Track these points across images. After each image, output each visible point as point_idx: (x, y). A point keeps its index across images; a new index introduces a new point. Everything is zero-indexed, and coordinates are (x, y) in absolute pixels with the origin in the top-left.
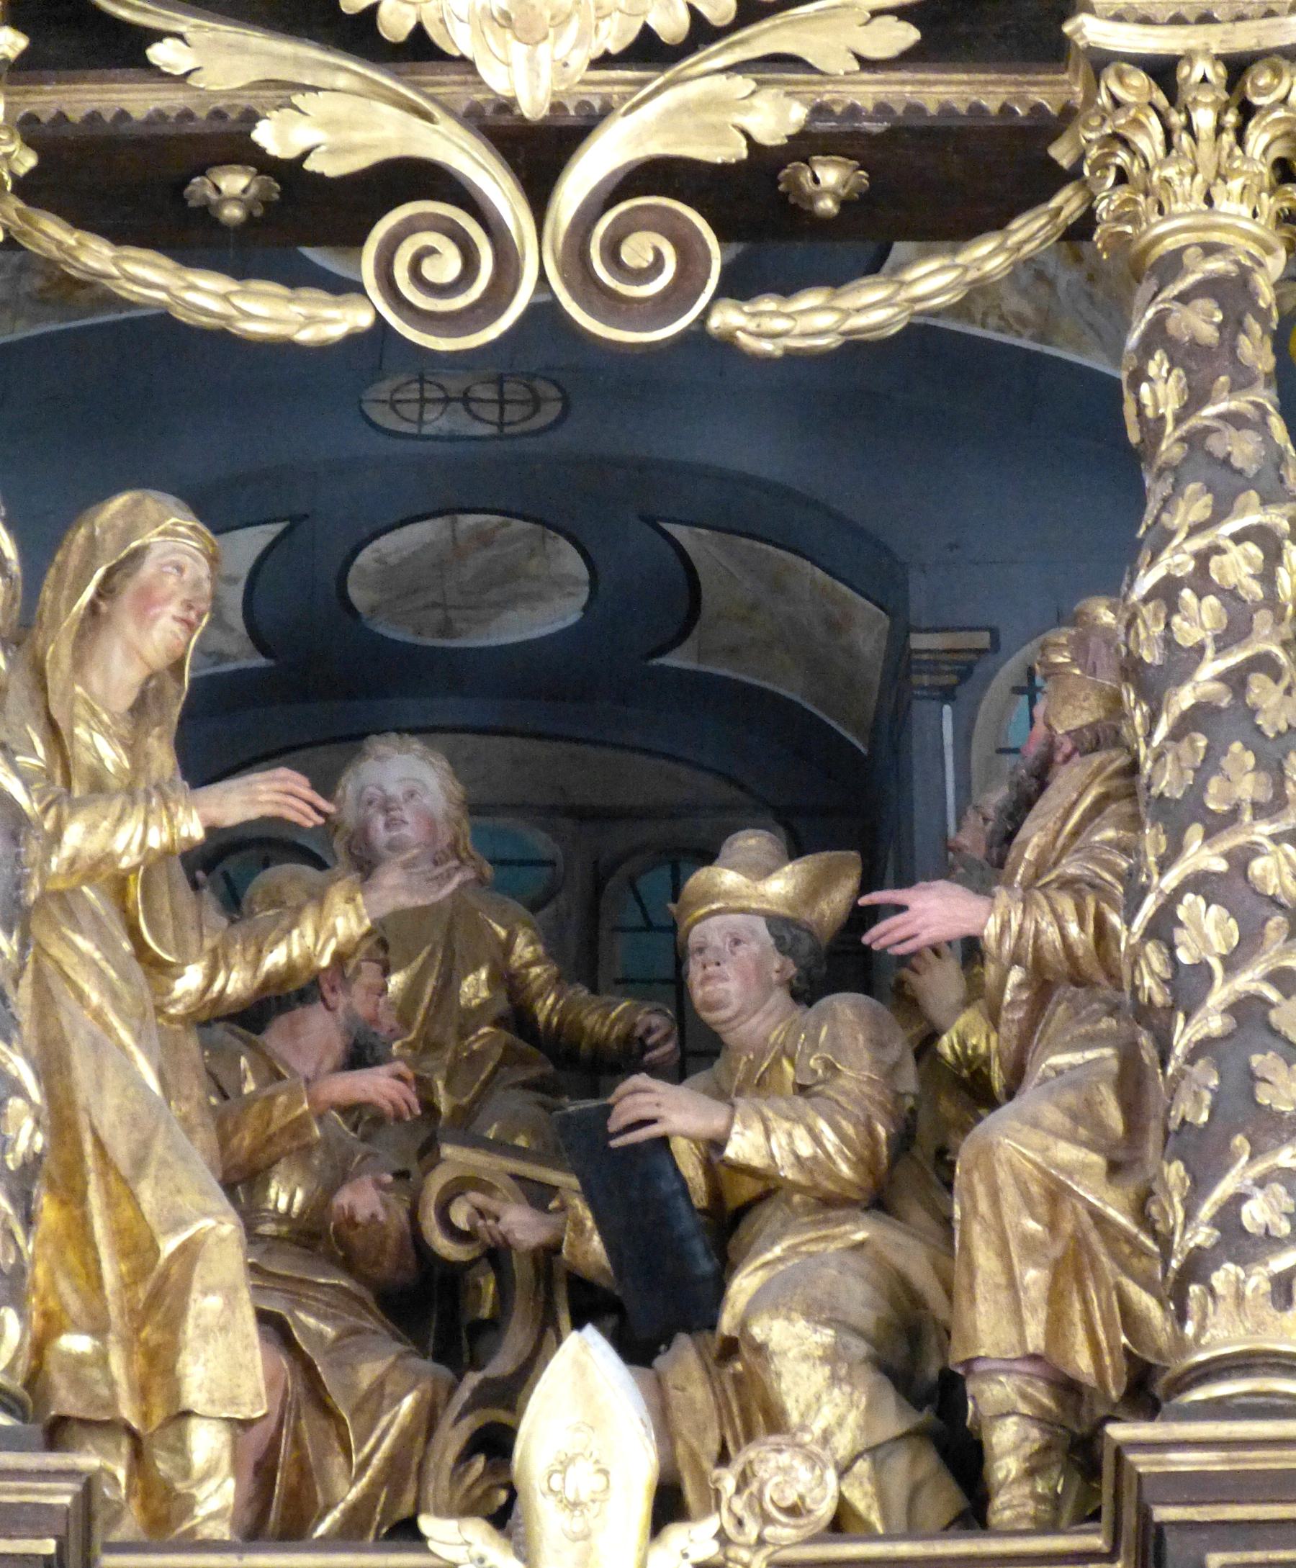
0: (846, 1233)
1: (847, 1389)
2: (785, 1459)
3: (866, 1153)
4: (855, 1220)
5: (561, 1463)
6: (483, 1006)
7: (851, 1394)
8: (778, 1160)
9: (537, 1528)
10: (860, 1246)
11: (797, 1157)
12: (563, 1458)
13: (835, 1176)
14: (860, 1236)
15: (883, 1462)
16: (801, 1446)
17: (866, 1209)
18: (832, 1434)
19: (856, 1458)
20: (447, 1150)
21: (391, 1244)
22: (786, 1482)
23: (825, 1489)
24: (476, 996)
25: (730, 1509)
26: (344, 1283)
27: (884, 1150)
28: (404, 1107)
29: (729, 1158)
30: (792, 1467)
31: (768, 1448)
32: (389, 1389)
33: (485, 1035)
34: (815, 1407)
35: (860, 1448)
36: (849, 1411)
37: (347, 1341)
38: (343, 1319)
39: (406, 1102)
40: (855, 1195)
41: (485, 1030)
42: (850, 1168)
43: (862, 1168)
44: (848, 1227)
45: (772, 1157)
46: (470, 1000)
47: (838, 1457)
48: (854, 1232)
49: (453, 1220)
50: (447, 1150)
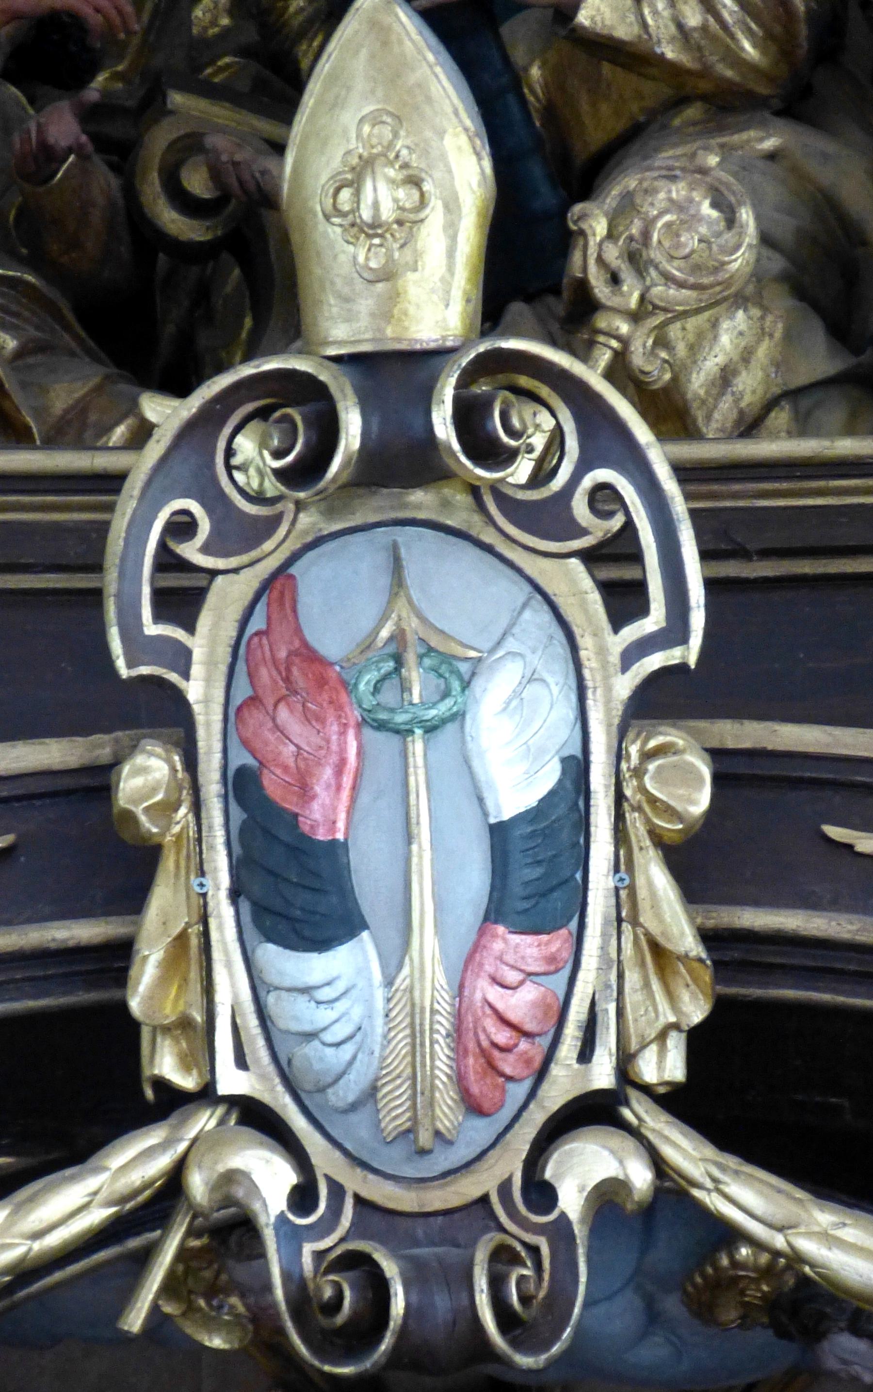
0: (748, 141)
1: (756, 312)
2: (678, 191)
3: (778, 29)
4: (762, 124)
5: (353, 169)
6: (226, 32)
7: (762, 318)
8: (652, 30)
9: (318, 271)
10: (772, 156)
11: (680, 26)
12: (355, 161)
13: (735, 58)
14: (770, 144)
15: (808, 414)
16: (704, 171)
17: (778, 113)
18: (735, 373)
19: (770, 405)
20: (177, 99)
21: (96, 217)
22: (683, 222)
23: (740, 234)
24: (214, 23)
25: (600, 260)
26: (30, 278)
27: (803, 30)
28: (118, 21)
29: (583, 28)
30: (691, 200)
31: (656, 174)
32: (93, 417)
33: (228, 66)
34: (710, 336)
35: (777, 390)
36: (759, 341)
37: (31, 360)
38: (24, 329)
39: (120, 12)
40: (763, 89)
41: (227, 60)
42: (755, 46)
43: (773, 48)
44: (752, 133)
45: (644, 25)
46: (205, 29)
47: (743, 404)
48: (761, 140)
49: (185, 184)
50: (177, 99)
